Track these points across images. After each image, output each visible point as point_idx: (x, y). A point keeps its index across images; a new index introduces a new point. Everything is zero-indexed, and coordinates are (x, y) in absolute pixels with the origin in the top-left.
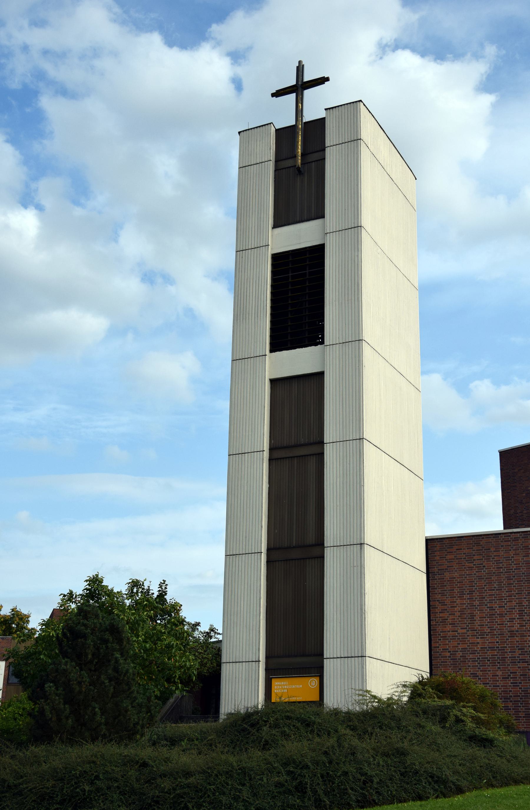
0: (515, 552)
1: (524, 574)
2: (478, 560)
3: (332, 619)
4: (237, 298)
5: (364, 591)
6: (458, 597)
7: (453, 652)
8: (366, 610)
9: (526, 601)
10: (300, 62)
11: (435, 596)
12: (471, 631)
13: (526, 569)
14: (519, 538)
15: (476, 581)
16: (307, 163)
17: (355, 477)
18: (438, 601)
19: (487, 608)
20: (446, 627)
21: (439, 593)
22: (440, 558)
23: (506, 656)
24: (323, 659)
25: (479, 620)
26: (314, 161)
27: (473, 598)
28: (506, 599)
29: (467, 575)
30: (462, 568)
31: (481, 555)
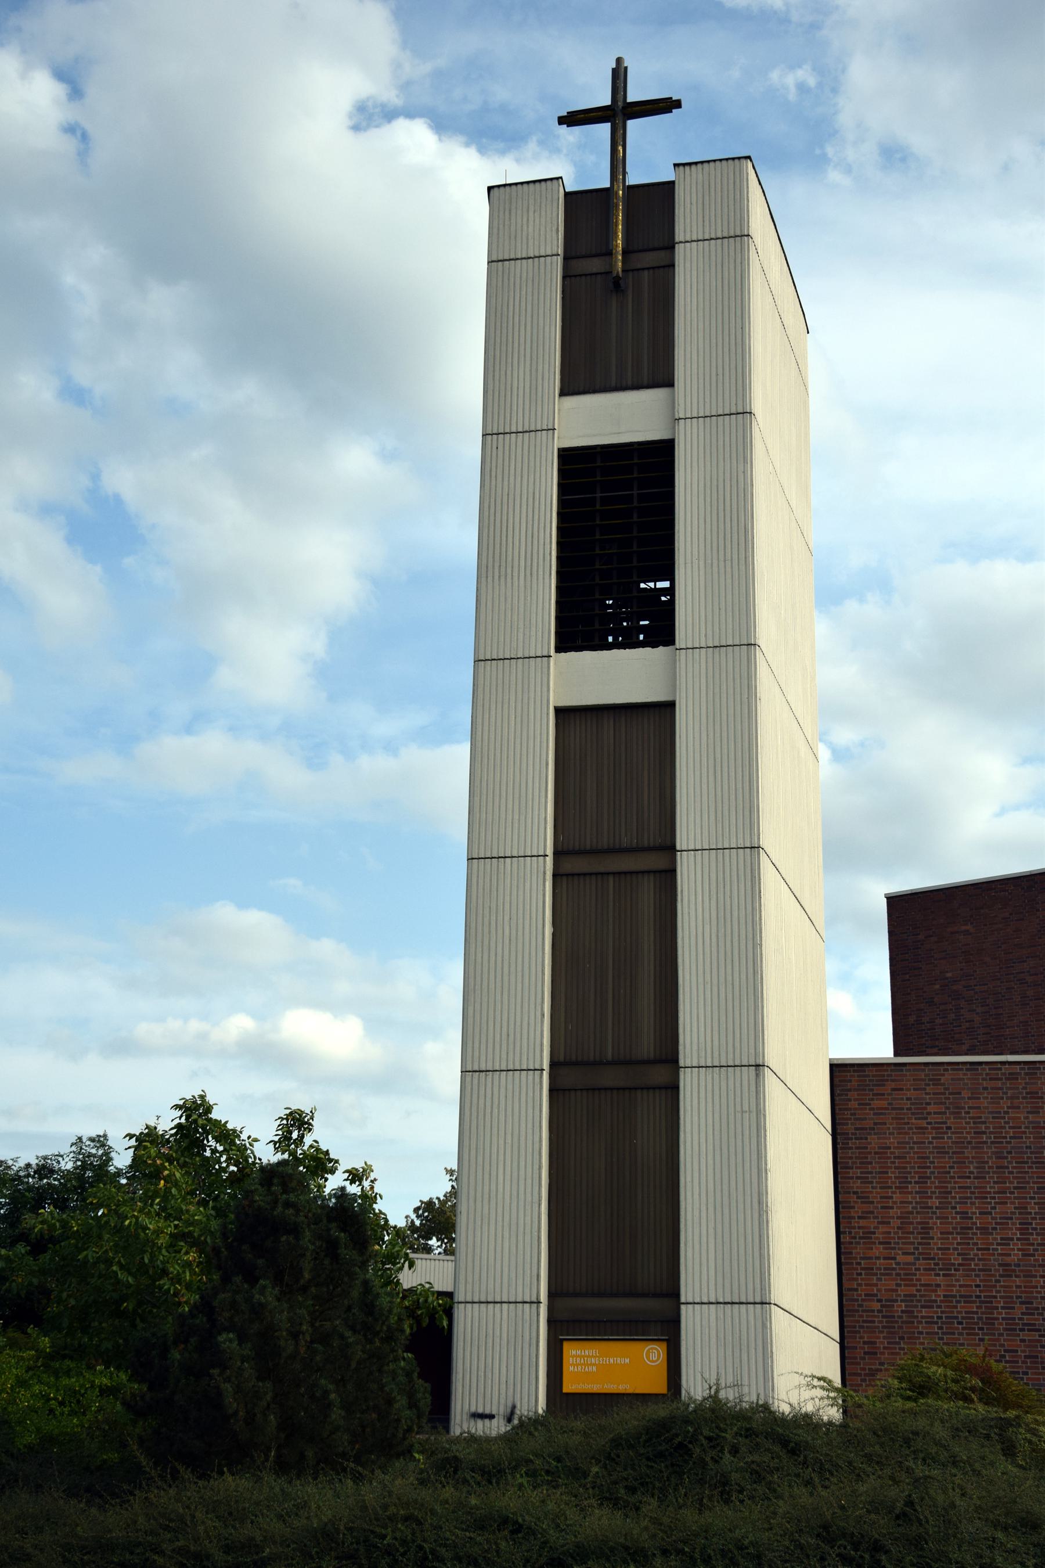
0: (1011, 1103)
1: (1030, 1148)
2: (935, 1113)
3: (696, 1220)
4: (486, 531)
5: (766, 1164)
6: (896, 1187)
7: (886, 1301)
8: (769, 1204)
9: (1035, 1203)
10: (619, 61)
11: (849, 1183)
12: (924, 1259)
13: (1034, 1138)
14: (1020, 1074)
15: (933, 1158)
16: (633, 270)
17: (743, 926)
18: (854, 1193)
19: (957, 1213)
20: (872, 1249)
21: (858, 1178)
22: (859, 1104)
23: (995, 1316)
24: (678, 1304)
25: (939, 1239)
26: (648, 269)
27: (927, 1193)
28: (994, 1198)
29: (914, 1143)
30: (904, 1128)
31: (941, 1103)
